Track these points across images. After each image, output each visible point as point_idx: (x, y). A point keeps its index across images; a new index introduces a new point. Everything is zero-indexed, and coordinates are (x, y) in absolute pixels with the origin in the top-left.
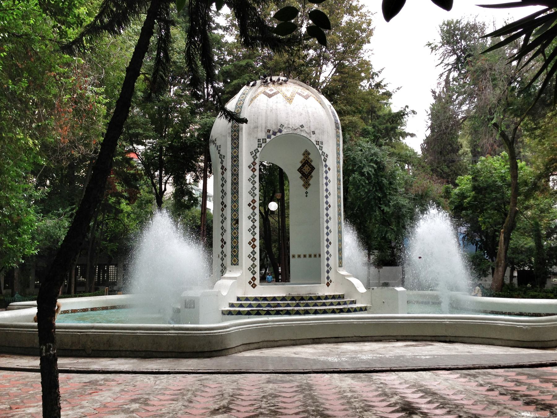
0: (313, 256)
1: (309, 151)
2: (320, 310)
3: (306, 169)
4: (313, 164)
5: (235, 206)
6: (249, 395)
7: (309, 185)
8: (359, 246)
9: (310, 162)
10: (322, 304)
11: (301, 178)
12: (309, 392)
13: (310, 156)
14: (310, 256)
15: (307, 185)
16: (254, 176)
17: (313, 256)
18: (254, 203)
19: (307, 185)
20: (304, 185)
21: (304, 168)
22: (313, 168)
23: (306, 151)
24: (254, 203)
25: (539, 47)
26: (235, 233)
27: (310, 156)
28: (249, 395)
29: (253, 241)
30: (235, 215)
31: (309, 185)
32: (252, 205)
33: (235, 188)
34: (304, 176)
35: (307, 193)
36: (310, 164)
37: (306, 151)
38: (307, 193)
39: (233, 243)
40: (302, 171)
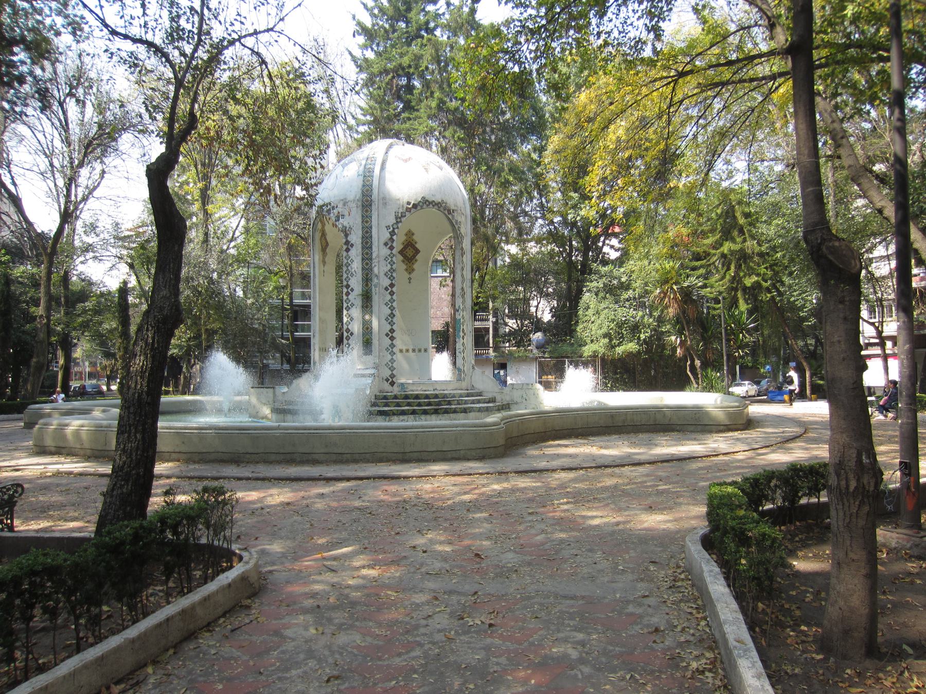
1: (413, 230)
3: (410, 252)
4: (417, 246)
5: (367, 264)
7: (413, 270)
8: (515, 455)
11: (403, 261)
12: (491, 345)
13: (414, 237)
15: (410, 270)
19: (410, 270)
20: (413, 234)
22: (417, 251)
23: (410, 231)
25: (349, 549)
26: (367, 254)
27: (414, 237)
31: (413, 270)
33: (367, 243)
35: (410, 279)
37: (410, 231)
38: (410, 279)
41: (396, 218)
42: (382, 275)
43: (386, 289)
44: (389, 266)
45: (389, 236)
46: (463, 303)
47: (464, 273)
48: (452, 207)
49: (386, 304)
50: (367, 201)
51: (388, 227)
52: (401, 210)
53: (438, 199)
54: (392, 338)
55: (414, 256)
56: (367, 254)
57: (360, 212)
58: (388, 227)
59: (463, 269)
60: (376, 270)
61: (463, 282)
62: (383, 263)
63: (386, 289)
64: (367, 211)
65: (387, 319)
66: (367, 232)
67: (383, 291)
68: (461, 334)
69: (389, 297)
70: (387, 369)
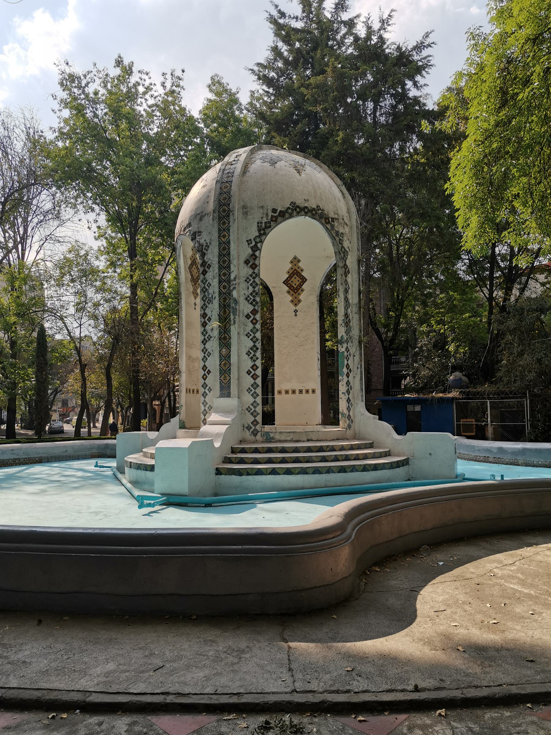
0: (310, 391)
2: (328, 446)
3: (295, 281)
6: (532, 661)
7: (300, 301)
9: (300, 271)
10: (320, 458)
11: (288, 292)
14: (307, 392)
16: (255, 386)
17: (310, 391)
18: (254, 370)
20: (299, 261)
21: (297, 277)
23: (295, 258)
24: (254, 370)
27: (300, 264)
28: (532, 661)
29: (253, 370)
30: (224, 236)
31: (300, 301)
32: (252, 317)
34: (299, 273)
35: (296, 311)
36: (300, 274)
37: (295, 258)
38: (296, 311)
39: (222, 289)
40: (294, 275)
41: (259, 230)
42: (242, 300)
43: (248, 317)
44: (251, 289)
45: (250, 251)
46: (348, 332)
47: (349, 296)
48: (332, 215)
49: (248, 335)
50: (224, 211)
51: (249, 242)
52: (265, 220)
53: (312, 204)
54: (204, 368)
55: (290, 277)
56: (225, 274)
57: (216, 225)
58: (249, 242)
59: (346, 291)
60: (235, 294)
61: (346, 308)
62: (243, 285)
63: (248, 317)
64: (224, 223)
65: (248, 354)
66: (224, 249)
67: (244, 319)
68: (345, 370)
69: (251, 326)
70: (249, 414)
